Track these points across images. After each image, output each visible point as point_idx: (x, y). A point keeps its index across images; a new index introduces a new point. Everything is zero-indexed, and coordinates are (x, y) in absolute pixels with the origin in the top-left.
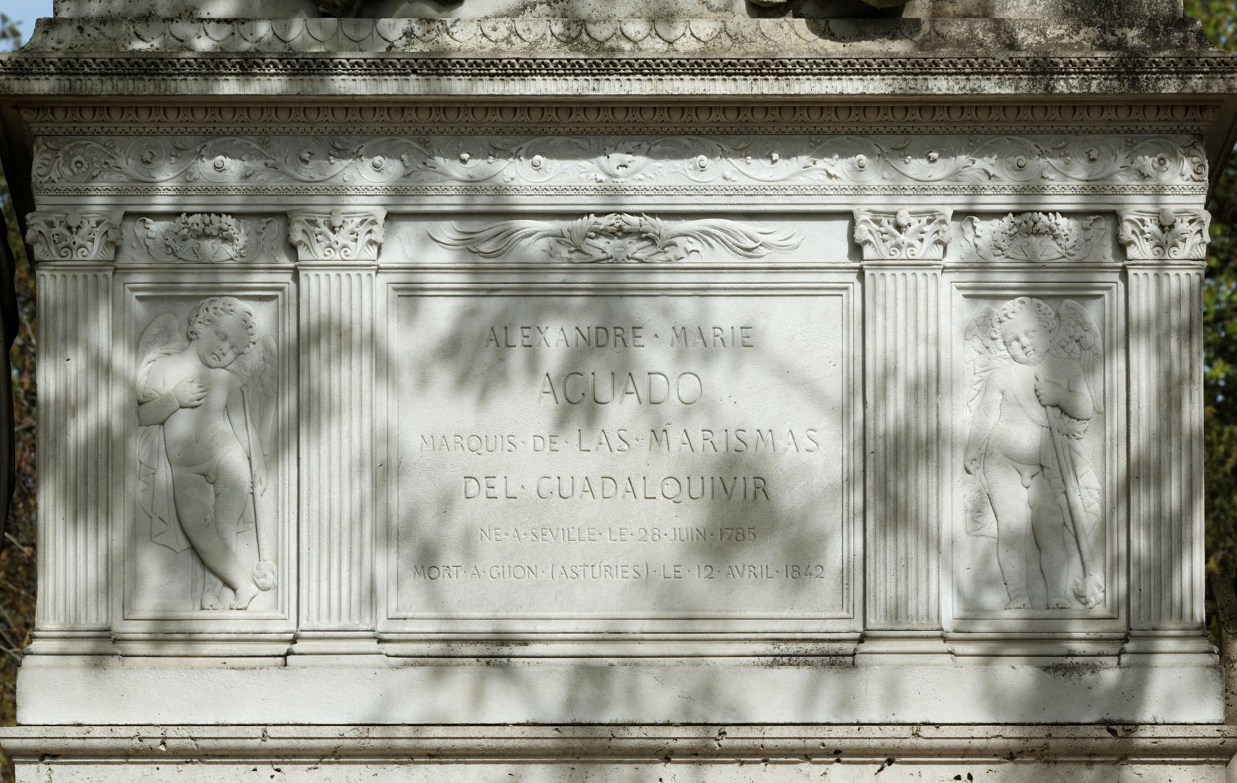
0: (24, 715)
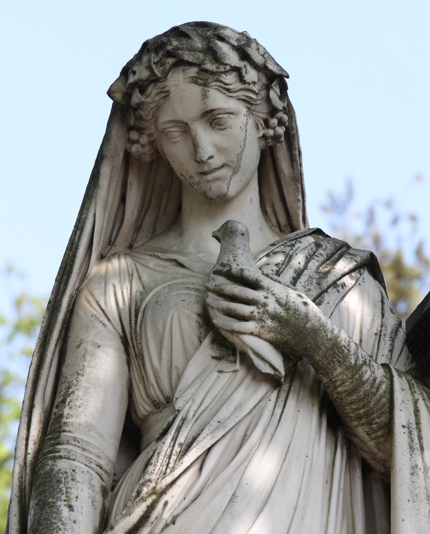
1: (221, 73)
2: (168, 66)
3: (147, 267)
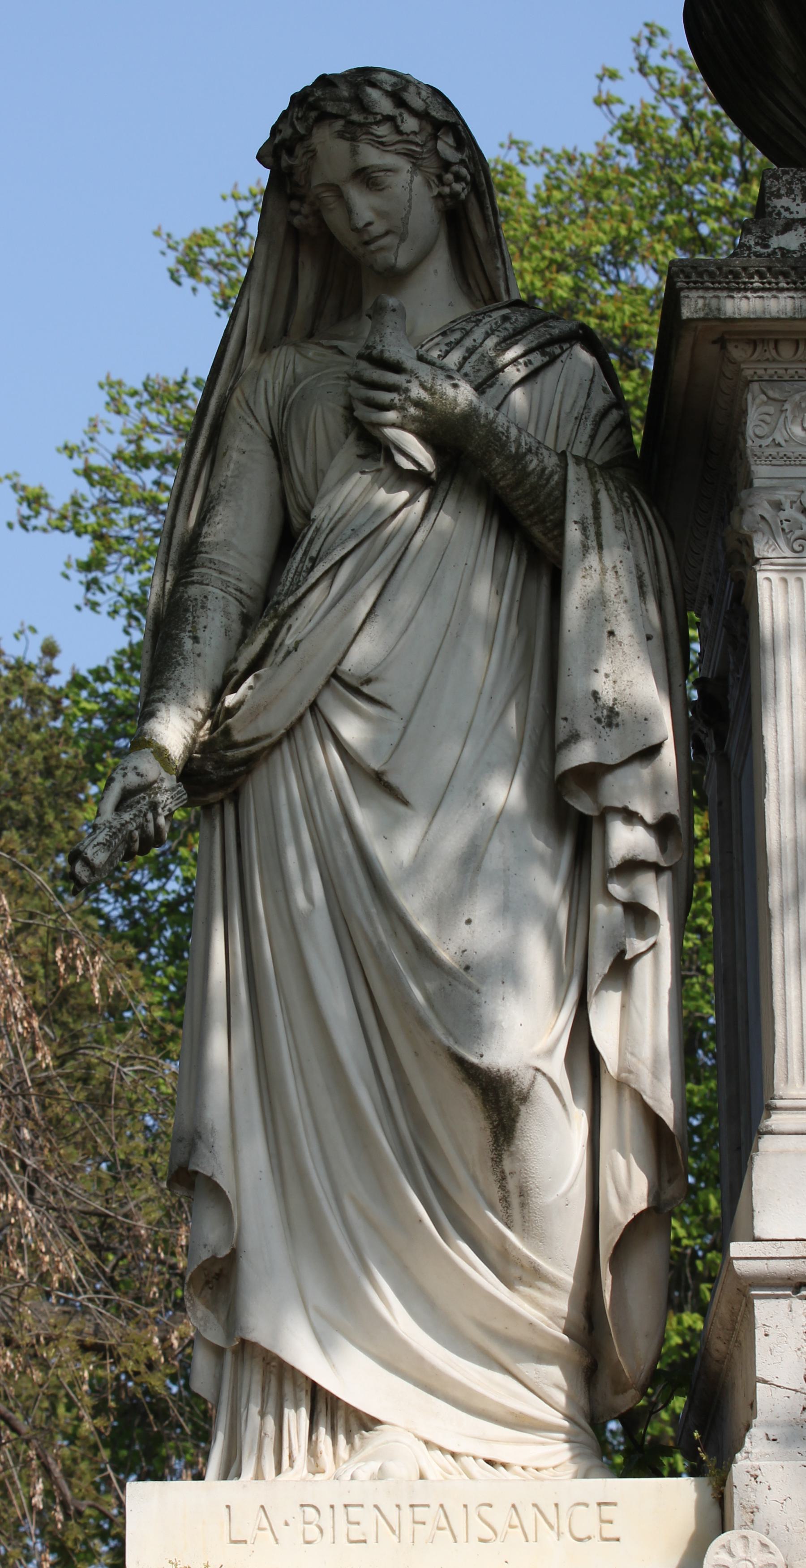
0: (761, 1227)
1: (371, 124)
2: (311, 120)
3: (306, 357)
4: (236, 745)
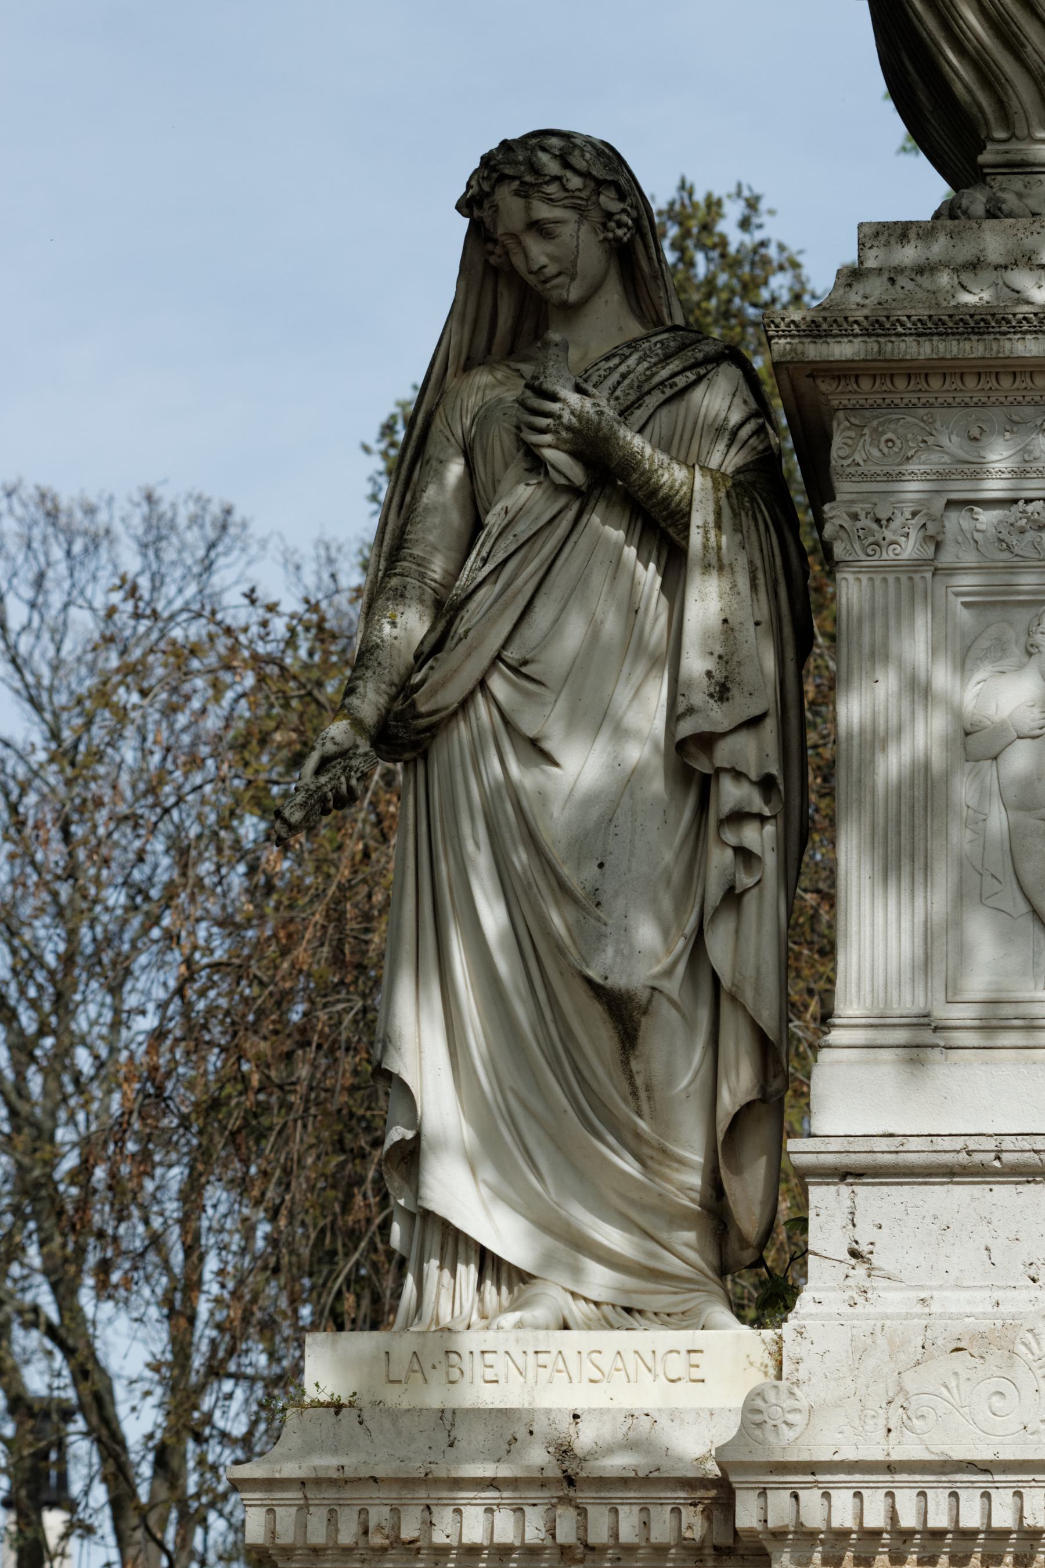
4: (421, 716)
